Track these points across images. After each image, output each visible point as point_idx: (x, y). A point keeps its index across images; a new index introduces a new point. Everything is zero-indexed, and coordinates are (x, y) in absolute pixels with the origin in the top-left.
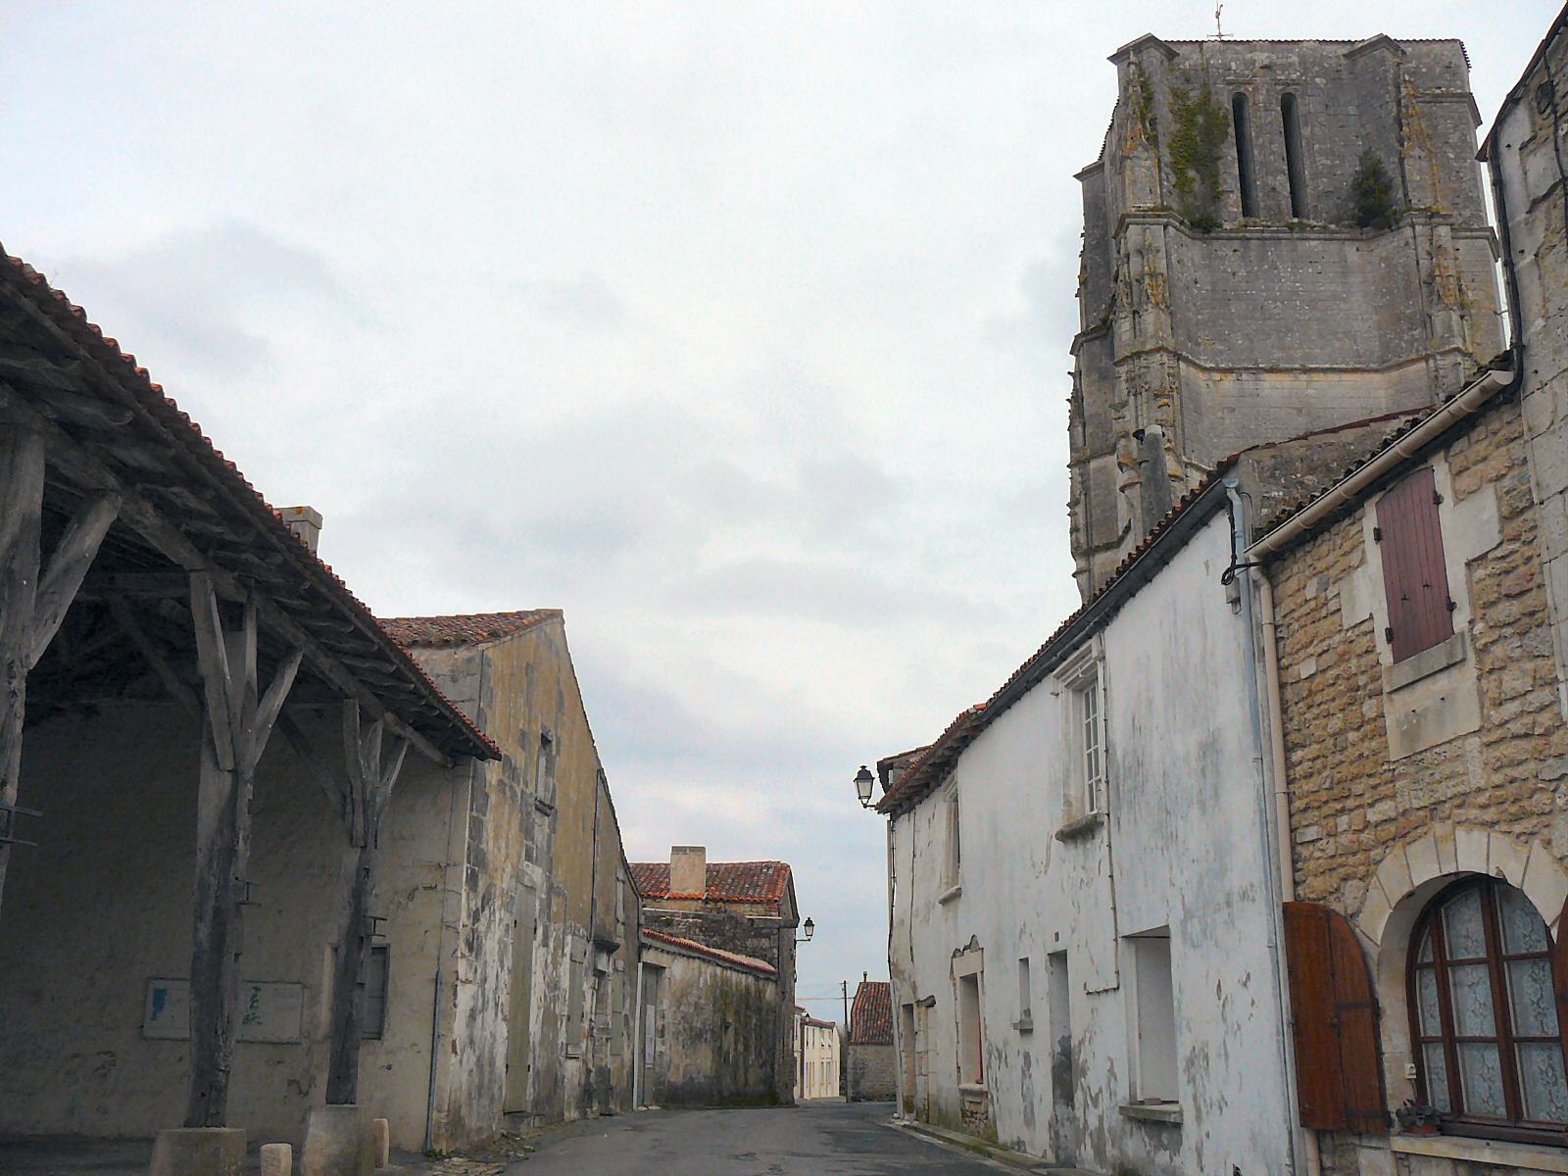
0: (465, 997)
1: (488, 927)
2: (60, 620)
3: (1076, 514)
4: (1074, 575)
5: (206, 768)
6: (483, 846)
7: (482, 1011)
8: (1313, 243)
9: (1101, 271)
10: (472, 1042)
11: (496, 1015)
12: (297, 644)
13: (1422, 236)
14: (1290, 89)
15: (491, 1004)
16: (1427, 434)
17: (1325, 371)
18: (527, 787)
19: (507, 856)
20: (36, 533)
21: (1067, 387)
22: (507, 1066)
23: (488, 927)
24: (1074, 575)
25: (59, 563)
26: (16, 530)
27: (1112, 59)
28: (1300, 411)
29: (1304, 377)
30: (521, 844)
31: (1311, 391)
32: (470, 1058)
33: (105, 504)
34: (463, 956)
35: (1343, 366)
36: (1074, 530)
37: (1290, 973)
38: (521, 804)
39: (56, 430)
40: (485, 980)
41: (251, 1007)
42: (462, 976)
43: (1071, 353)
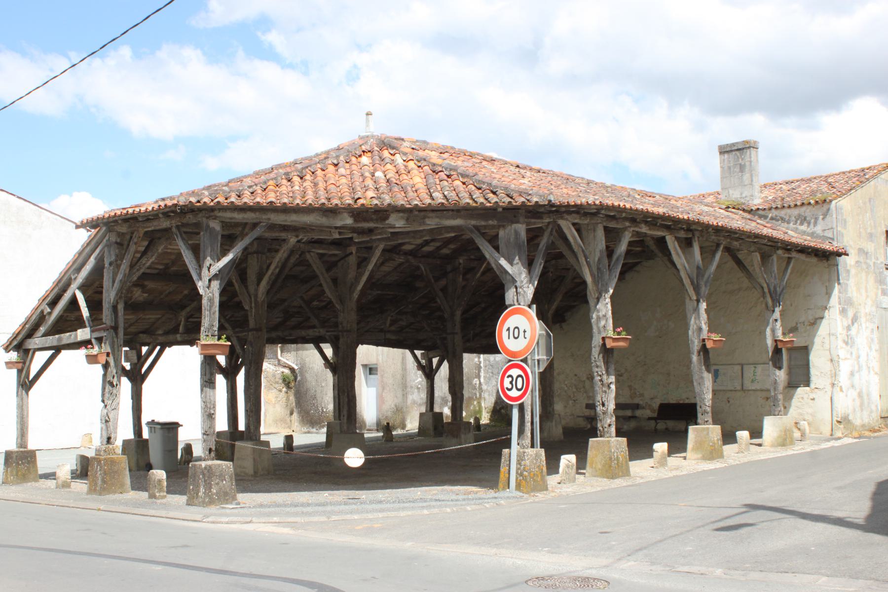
0: (845, 368)
1: (858, 332)
2: (617, 277)
5: (687, 301)
6: (849, 295)
7: (859, 371)
10: (853, 386)
11: (869, 372)
12: (720, 242)
13: (69, 59)
15: (864, 367)
16: (23, 336)
18: (877, 259)
19: (867, 296)
20: (605, 254)
22: (880, 396)
23: (858, 332)
25: (615, 257)
26: (599, 255)
30: (877, 288)
32: (853, 394)
33: (627, 233)
34: (842, 348)
38: (874, 269)
39: (605, 219)
40: (859, 357)
41: (754, 375)
42: (841, 356)
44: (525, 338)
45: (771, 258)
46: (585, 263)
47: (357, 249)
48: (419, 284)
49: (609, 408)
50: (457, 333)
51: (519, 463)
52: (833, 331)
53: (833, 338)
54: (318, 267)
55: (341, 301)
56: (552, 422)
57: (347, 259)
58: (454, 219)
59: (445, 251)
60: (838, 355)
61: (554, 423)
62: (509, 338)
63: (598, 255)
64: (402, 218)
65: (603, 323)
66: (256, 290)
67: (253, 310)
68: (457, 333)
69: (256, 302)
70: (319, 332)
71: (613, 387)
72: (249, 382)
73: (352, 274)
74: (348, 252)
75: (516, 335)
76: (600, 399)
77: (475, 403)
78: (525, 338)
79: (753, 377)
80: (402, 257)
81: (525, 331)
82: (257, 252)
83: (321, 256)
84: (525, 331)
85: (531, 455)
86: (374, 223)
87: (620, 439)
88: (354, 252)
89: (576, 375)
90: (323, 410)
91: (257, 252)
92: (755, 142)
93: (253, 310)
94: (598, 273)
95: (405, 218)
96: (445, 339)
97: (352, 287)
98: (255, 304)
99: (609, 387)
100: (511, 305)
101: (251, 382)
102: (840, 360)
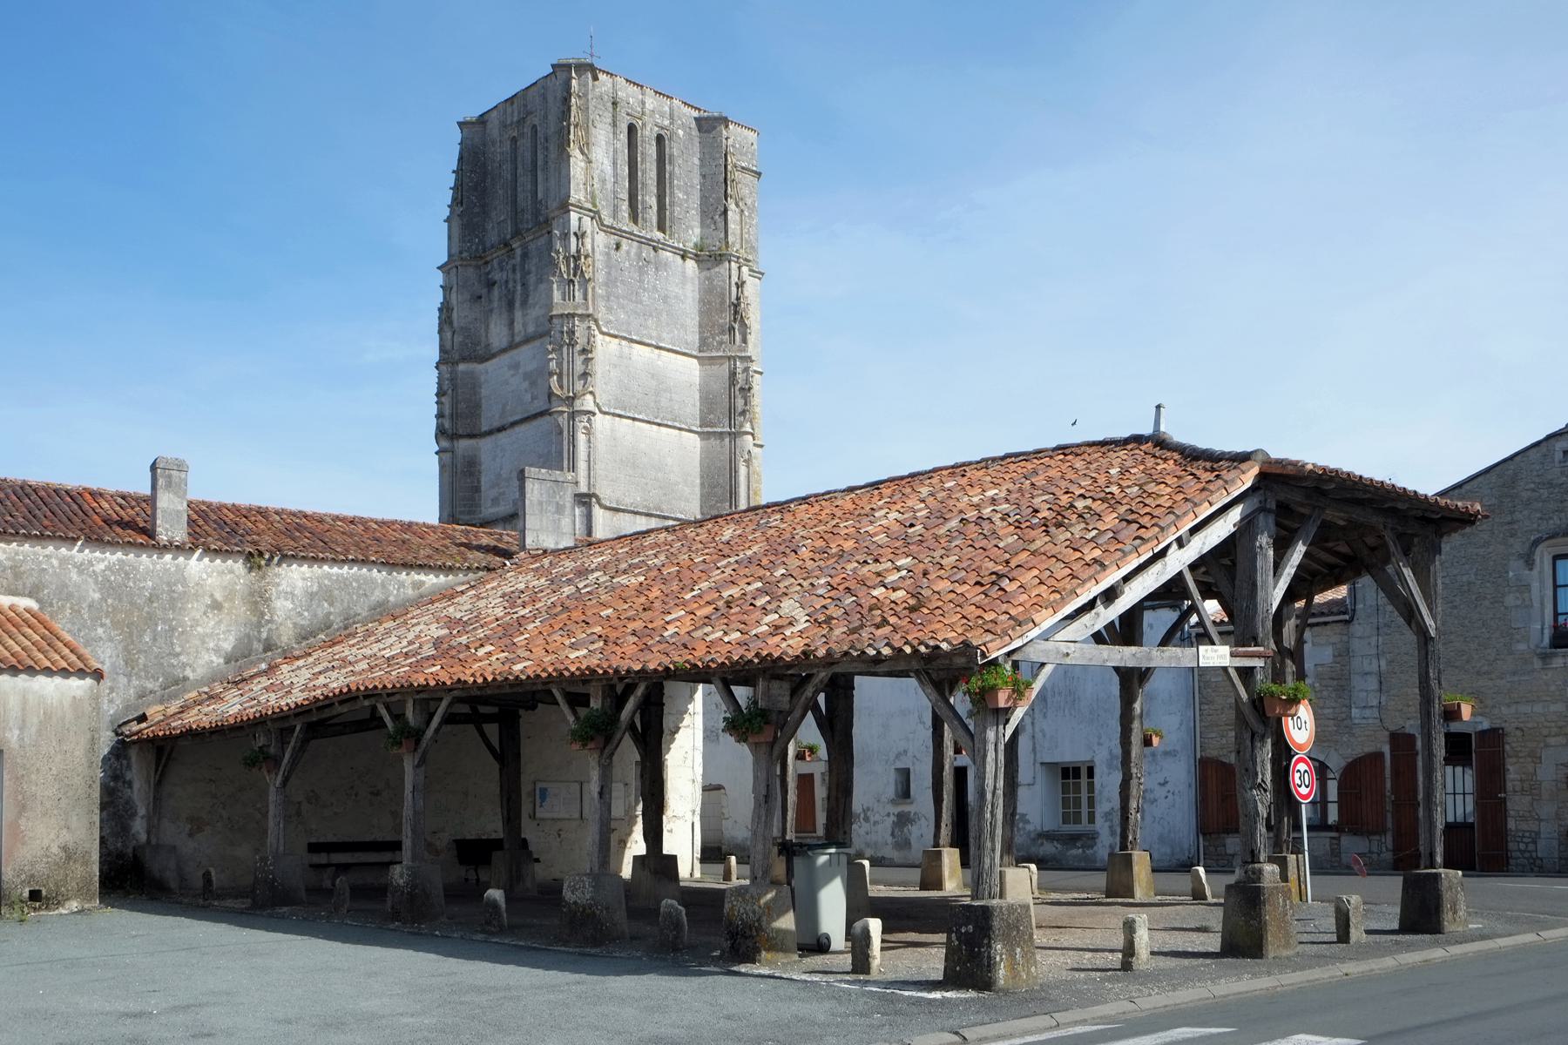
3: (442, 403)
4: (436, 453)
8: (668, 254)
9: (476, 210)
14: (662, 132)
17: (669, 350)
21: (438, 298)
24: (436, 453)
27: (461, 124)
28: (653, 375)
29: (657, 351)
31: (659, 363)
35: (678, 349)
36: (440, 416)
37: (1169, 1029)
43: (553, 66)
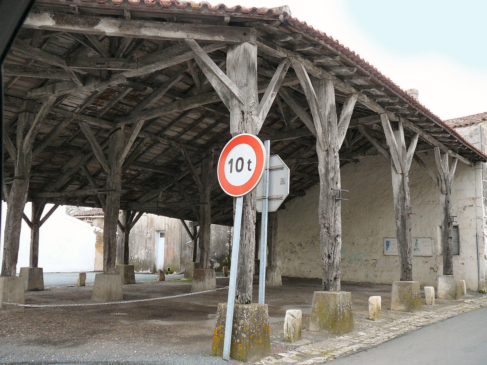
2: (345, 134)
20: (335, 109)
39: (335, 78)
41: (416, 245)
44: (250, 170)
45: (446, 154)
46: (316, 112)
47: (126, 125)
48: (183, 169)
49: (336, 261)
50: (207, 203)
51: (235, 320)
52: (479, 215)
53: (478, 220)
54: (90, 135)
55: (109, 166)
56: (274, 272)
57: (116, 132)
58: (175, 31)
59: (200, 141)
60: (483, 233)
61: (276, 274)
62: (231, 172)
63: (328, 109)
64: (114, 24)
65: (331, 175)
66: (22, 143)
67: (18, 161)
68: (207, 203)
69: (22, 155)
70: (94, 192)
71: (339, 240)
72: (8, 223)
73: (119, 144)
74: (117, 127)
75: (239, 168)
76: (326, 251)
77: (226, 258)
78: (250, 170)
79: (416, 247)
80: (166, 141)
81: (249, 162)
82: (25, 111)
83: (93, 128)
84: (249, 162)
85: (252, 312)
86: (80, 27)
87: (345, 293)
88: (122, 128)
89: (291, 243)
90: (131, 259)
91: (25, 111)
92: (417, 91)
93: (18, 161)
94: (328, 127)
95: (119, 26)
96: (198, 207)
97: (119, 154)
98: (20, 156)
99: (335, 239)
100: (236, 134)
101: (10, 223)
102: (485, 236)
